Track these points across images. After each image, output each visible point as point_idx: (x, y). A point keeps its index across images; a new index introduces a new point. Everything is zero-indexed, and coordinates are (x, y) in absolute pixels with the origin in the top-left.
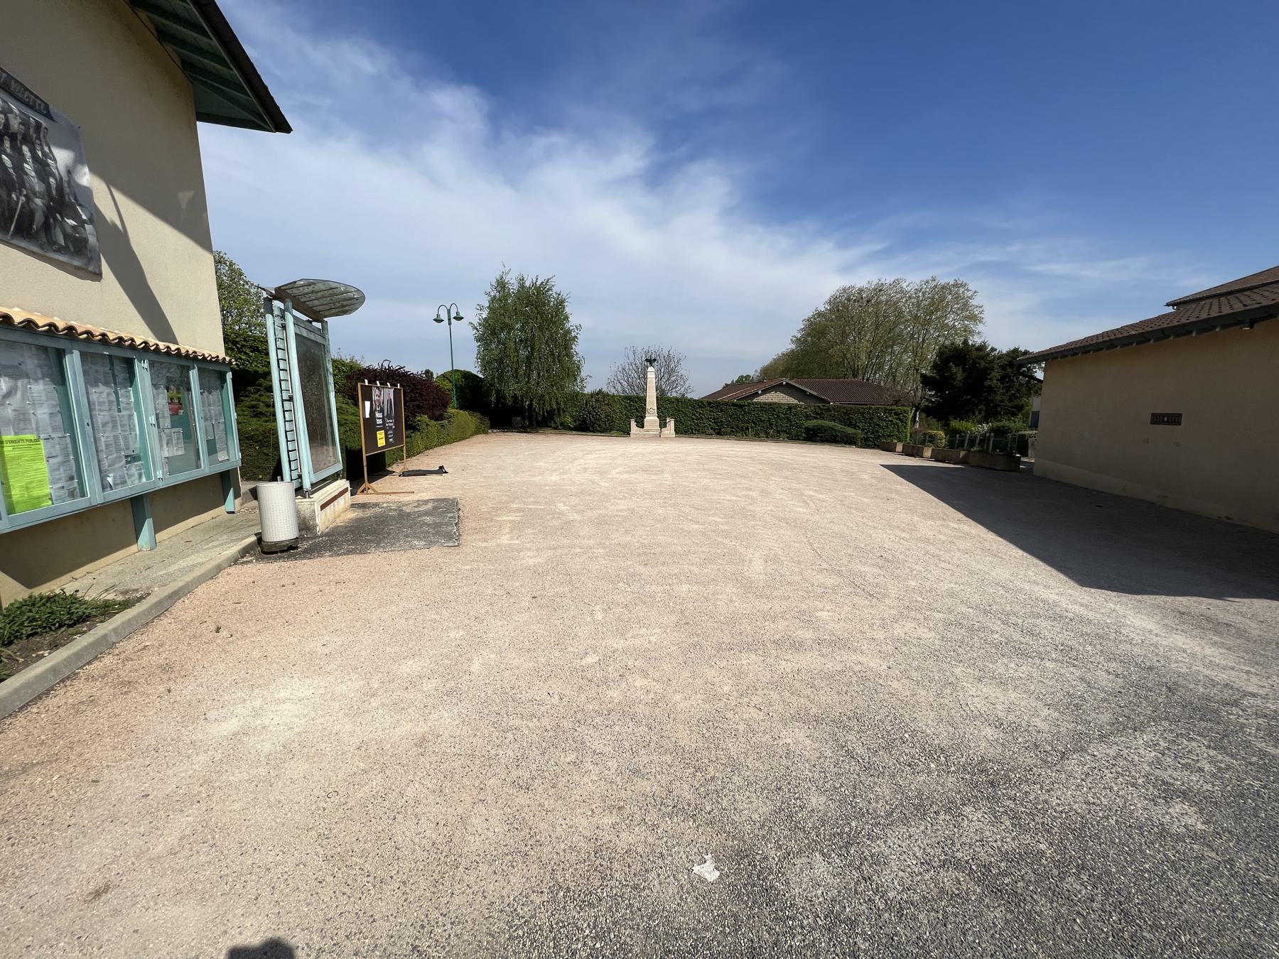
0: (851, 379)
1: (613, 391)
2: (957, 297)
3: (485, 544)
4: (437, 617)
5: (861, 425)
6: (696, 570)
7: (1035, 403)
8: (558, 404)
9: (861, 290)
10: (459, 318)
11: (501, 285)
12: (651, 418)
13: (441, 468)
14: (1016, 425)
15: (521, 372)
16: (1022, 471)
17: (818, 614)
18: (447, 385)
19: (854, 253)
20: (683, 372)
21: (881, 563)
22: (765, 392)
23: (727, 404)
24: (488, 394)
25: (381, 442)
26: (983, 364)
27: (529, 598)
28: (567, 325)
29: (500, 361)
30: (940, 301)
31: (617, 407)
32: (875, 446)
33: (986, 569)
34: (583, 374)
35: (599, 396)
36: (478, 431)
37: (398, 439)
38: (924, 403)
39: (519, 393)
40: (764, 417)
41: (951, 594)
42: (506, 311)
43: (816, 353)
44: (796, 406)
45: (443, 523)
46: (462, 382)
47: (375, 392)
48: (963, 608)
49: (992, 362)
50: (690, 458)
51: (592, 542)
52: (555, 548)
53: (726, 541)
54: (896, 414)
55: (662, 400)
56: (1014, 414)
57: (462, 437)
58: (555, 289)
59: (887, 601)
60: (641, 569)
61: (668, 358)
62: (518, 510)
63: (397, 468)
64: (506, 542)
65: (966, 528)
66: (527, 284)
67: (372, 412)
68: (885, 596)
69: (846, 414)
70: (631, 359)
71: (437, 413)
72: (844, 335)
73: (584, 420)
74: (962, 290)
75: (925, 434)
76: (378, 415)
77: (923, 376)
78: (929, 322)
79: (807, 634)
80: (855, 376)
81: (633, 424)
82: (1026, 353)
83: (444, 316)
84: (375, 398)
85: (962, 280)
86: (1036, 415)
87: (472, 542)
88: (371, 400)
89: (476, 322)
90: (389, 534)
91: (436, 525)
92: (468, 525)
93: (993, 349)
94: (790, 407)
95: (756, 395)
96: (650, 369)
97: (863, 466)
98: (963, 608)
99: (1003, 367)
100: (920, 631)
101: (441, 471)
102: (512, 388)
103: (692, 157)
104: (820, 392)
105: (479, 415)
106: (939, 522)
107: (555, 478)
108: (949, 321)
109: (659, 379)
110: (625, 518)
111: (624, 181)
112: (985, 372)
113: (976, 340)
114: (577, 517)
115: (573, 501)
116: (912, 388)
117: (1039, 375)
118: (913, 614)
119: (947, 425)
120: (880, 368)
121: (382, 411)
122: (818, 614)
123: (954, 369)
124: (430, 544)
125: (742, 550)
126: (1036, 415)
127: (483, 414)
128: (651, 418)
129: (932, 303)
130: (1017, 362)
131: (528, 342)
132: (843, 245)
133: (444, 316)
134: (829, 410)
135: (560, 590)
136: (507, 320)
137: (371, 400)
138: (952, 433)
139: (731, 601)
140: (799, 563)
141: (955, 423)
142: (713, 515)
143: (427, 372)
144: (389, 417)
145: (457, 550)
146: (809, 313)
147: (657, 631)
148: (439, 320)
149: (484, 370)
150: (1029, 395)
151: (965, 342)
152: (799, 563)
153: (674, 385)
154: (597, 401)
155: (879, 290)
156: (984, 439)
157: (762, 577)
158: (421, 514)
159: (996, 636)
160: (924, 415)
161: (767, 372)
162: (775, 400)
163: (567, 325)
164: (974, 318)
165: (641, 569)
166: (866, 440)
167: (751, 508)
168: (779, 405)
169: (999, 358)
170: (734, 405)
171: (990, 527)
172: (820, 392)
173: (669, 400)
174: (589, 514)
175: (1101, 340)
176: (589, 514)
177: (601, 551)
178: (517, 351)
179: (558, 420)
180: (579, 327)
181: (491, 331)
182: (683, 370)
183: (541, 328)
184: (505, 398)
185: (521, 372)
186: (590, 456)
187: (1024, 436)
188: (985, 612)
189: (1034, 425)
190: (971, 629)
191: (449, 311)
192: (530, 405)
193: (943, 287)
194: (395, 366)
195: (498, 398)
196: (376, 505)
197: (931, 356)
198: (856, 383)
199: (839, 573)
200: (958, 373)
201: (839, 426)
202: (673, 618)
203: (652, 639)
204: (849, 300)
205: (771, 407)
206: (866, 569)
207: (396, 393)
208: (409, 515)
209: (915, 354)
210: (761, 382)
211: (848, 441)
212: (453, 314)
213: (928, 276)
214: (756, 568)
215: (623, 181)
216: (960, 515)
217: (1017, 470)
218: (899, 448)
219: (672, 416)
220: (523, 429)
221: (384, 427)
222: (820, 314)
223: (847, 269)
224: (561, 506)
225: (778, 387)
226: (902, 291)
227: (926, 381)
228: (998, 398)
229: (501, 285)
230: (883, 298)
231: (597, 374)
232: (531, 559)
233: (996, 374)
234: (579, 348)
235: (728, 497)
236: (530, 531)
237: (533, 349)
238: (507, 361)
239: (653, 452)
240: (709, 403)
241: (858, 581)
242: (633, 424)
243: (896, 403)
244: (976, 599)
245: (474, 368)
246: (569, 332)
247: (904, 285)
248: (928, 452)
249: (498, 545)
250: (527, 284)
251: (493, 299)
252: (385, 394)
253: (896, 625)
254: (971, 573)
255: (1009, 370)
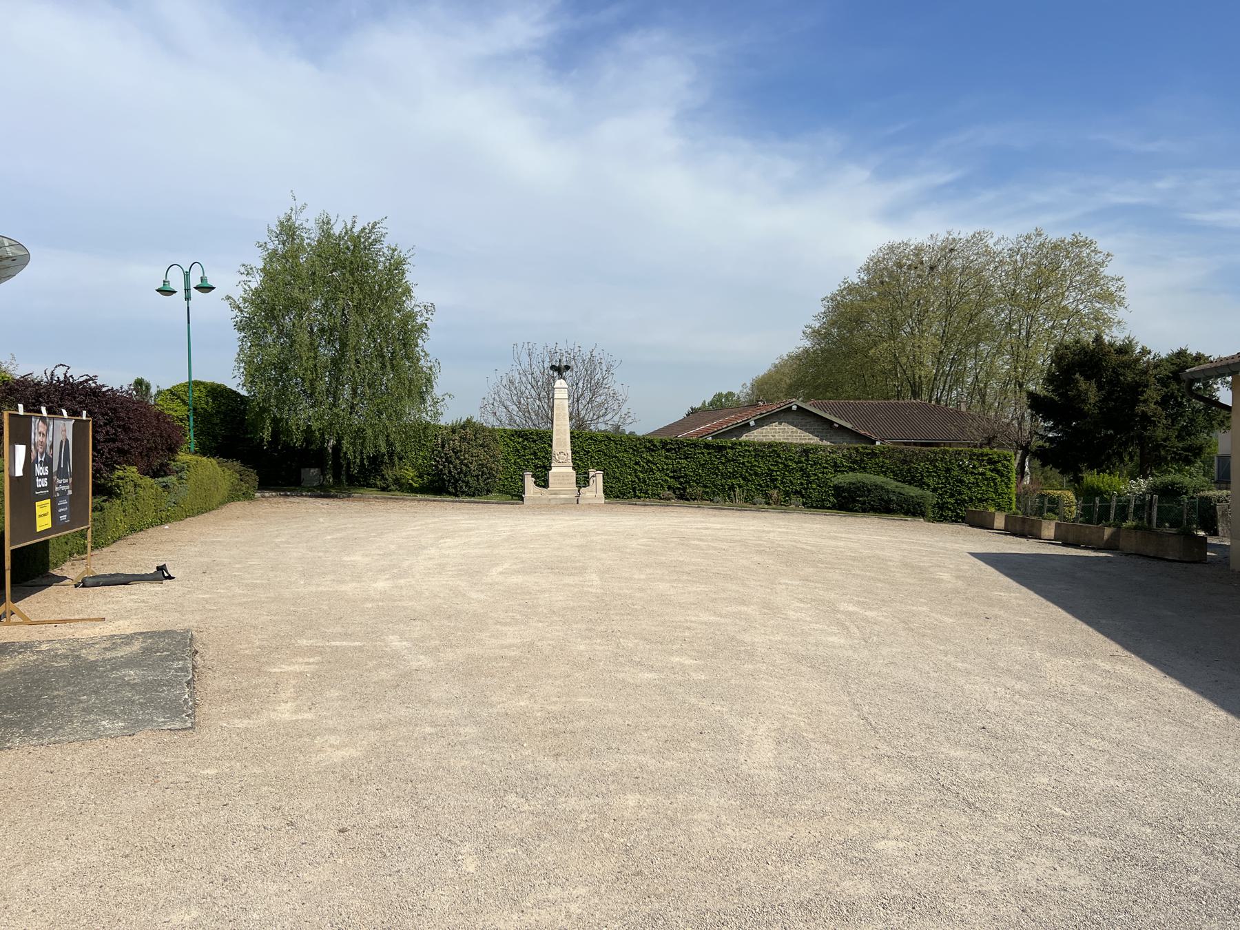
0: (909, 400)
1: (496, 424)
2: (1080, 264)
3: (243, 723)
4: (146, 881)
5: (930, 481)
6: (652, 763)
7: (1222, 442)
8: (389, 444)
9: (919, 251)
10: (205, 288)
11: (288, 231)
12: (562, 470)
13: (161, 569)
14: (1191, 479)
15: (322, 386)
16: (1212, 562)
17: (880, 845)
18: (178, 410)
19: (907, 186)
20: (617, 387)
21: (983, 741)
22: (761, 422)
23: (695, 445)
24: (257, 426)
25: (43, 521)
26: (1130, 377)
27: (332, 833)
28: (409, 305)
29: (282, 367)
30: (1050, 271)
31: (499, 449)
32: (957, 519)
33: (1167, 749)
34: (437, 391)
35: (468, 431)
36: (235, 496)
37: (77, 515)
38: (1036, 443)
39: (316, 426)
40: (762, 467)
41: (1112, 799)
42: (297, 277)
43: (847, 355)
44: (816, 449)
45: (162, 681)
46: (207, 405)
47: (37, 427)
48: (1134, 827)
49: (1145, 372)
50: (634, 544)
51: (454, 712)
52: (383, 727)
53: (703, 704)
54: (991, 462)
55: (579, 437)
56: (1188, 462)
57: (203, 507)
58: (386, 241)
59: (1001, 817)
60: (550, 765)
61: (591, 363)
62: (312, 651)
63: (72, 570)
64: (287, 716)
65: (1126, 670)
66: (337, 230)
67: (29, 465)
68: (996, 806)
69: (904, 462)
70: (525, 365)
71: (156, 463)
72: (894, 325)
73: (440, 473)
74: (1085, 252)
75: (1042, 496)
76: (40, 470)
77: (1031, 395)
78: (1035, 304)
79: (859, 888)
80: (915, 394)
81: (529, 481)
82: (1199, 358)
83: (177, 283)
84: (36, 438)
85: (1086, 234)
86: (1225, 461)
87: (223, 721)
88: (26, 440)
89: (238, 294)
90: (51, 707)
91: (149, 687)
92: (213, 682)
93: (1145, 352)
94: (806, 451)
95: (746, 427)
96: (560, 383)
97: (942, 553)
98: (1134, 827)
99: (1163, 382)
100: (1063, 873)
101: (162, 574)
102: (303, 417)
103: (627, 25)
104: (851, 429)
105: (237, 465)
106: (1079, 661)
107: (382, 584)
108: (1069, 301)
109: (575, 400)
110: (514, 661)
111: (513, 58)
112: (1135, 390)
113: (1114, 335)
114: (426, 662)
115: (418, 629)
116: (1014, 415)
117: (1224, 395)
118: (1047, 841)
119: (1078, 480)
120: (958, 381)
121: (48, 462)
122: (880, 845)
123: (1083, 385)
124: (134, 726)
125: (733, 721)
126: (1225, 461)
127: (245, 462)
128: (562, 470)
129: (1038, 273)
130: (1184, 375)
131: (336, 334)
132: (886, 173)
133: (177, 283)
134: (873, 455)
135: (394, 813)
136: (296, 293)
137: (26, 440)
138: (1088, 494)
139: (719, 825)
140: (837, 744)
141: (1091, 478)
142: (680, 652)
143: (139, 383)
144: (62, 473)
145: (192, 737)
146: (833, 288)
147: (582, 891)
148: (166, 291)
149: (251, 380)
150: (1210, 428)
151: (1098, 339)
152: (837, 744)
153: (603, 409)
154: (463, 439)
155: (949, 249)
156: (1142, 507)
157: (773, 774)
158: (118, 665)
159: (1196, 878)
160: (1037, 463)
161: (764, 388)
162: (769, 438)
163: (409, 305)
164: (1108, 297)
165: (550, 765)
166: (942, 507)
167: (747, 638)
168: (786, 447)
169: (1156, 366)
170: (707, 446)
171: (1168, 669)
172: (851, 429)
173: (592, 438)
174: (449, 655)
175: (1230, 361)
176: (449, 655)
177: (471, 730)
178: (313, 347)
179: (389, 473)
180: (430, 308)
181: (267, 313)
182: (616, 383)
183: (359, 308)
184: (288, 432)
185: (322, 386)
186: (449, 542)
187: (1208, 499)
188: (1174, 832)
189: (1224, 480)
190: (1150, 866)
191: (187, 276)
192: (337, 448)
193: (1055, 247)
194: (77, 374)
195: (275, 434)
196: (27, 646)
197: (1043, 360)
198: (918, 406)
199: (911, 763)
200: (1090, 392)
201: (892, 484)
202: (612, 863)
203: (573, 908)
204: (900, 266)
205: (773, 450)
206: (958, 753)
207: (79, 429)
208: (93, 666)
209: (1016, 357)
210: (753, 404)
211: (911, 510)
212: (195, 281)
213: (1027, 227)
214: (761, 756)
215: (513, 58)
216: (1114, 647)
217: (1203, 560)
218: (1000, 521)
219: (598, 466)
220: (322, 491)
221: (50, 494)
222: (851, 289)
223: (894, 213)
224: (395, 642)
225: (784, 415)
226: (987, 253)
227: (1037, 403)
228: (1160, 433)
229: (288, 231)
230: (957, 263)
231: (463, 389)
232: (336, 751)
233: (1153, 393)
234: (431, 346)
235: (705, 617)
236: (334, 693)
237: (344, 345)
238: (294, 367)
239: (563, 534)
240: (664, 444)
241: (946, 777)
242: (529, 481)
243: (990, 441)
244: (1155, 807)
245: (232, 378)
246: (411, 316)
247: (991, 242)
248: (1049, 530)
249: (272, 724)
250: (337, 230)
251: (272, 256)
252: (56, 431)
253: (1019, 864)
254: (1143, 755)
255: (1174, 386)
